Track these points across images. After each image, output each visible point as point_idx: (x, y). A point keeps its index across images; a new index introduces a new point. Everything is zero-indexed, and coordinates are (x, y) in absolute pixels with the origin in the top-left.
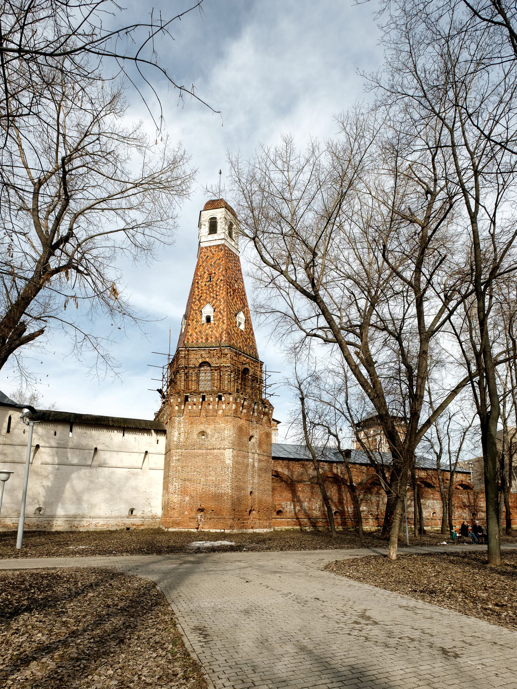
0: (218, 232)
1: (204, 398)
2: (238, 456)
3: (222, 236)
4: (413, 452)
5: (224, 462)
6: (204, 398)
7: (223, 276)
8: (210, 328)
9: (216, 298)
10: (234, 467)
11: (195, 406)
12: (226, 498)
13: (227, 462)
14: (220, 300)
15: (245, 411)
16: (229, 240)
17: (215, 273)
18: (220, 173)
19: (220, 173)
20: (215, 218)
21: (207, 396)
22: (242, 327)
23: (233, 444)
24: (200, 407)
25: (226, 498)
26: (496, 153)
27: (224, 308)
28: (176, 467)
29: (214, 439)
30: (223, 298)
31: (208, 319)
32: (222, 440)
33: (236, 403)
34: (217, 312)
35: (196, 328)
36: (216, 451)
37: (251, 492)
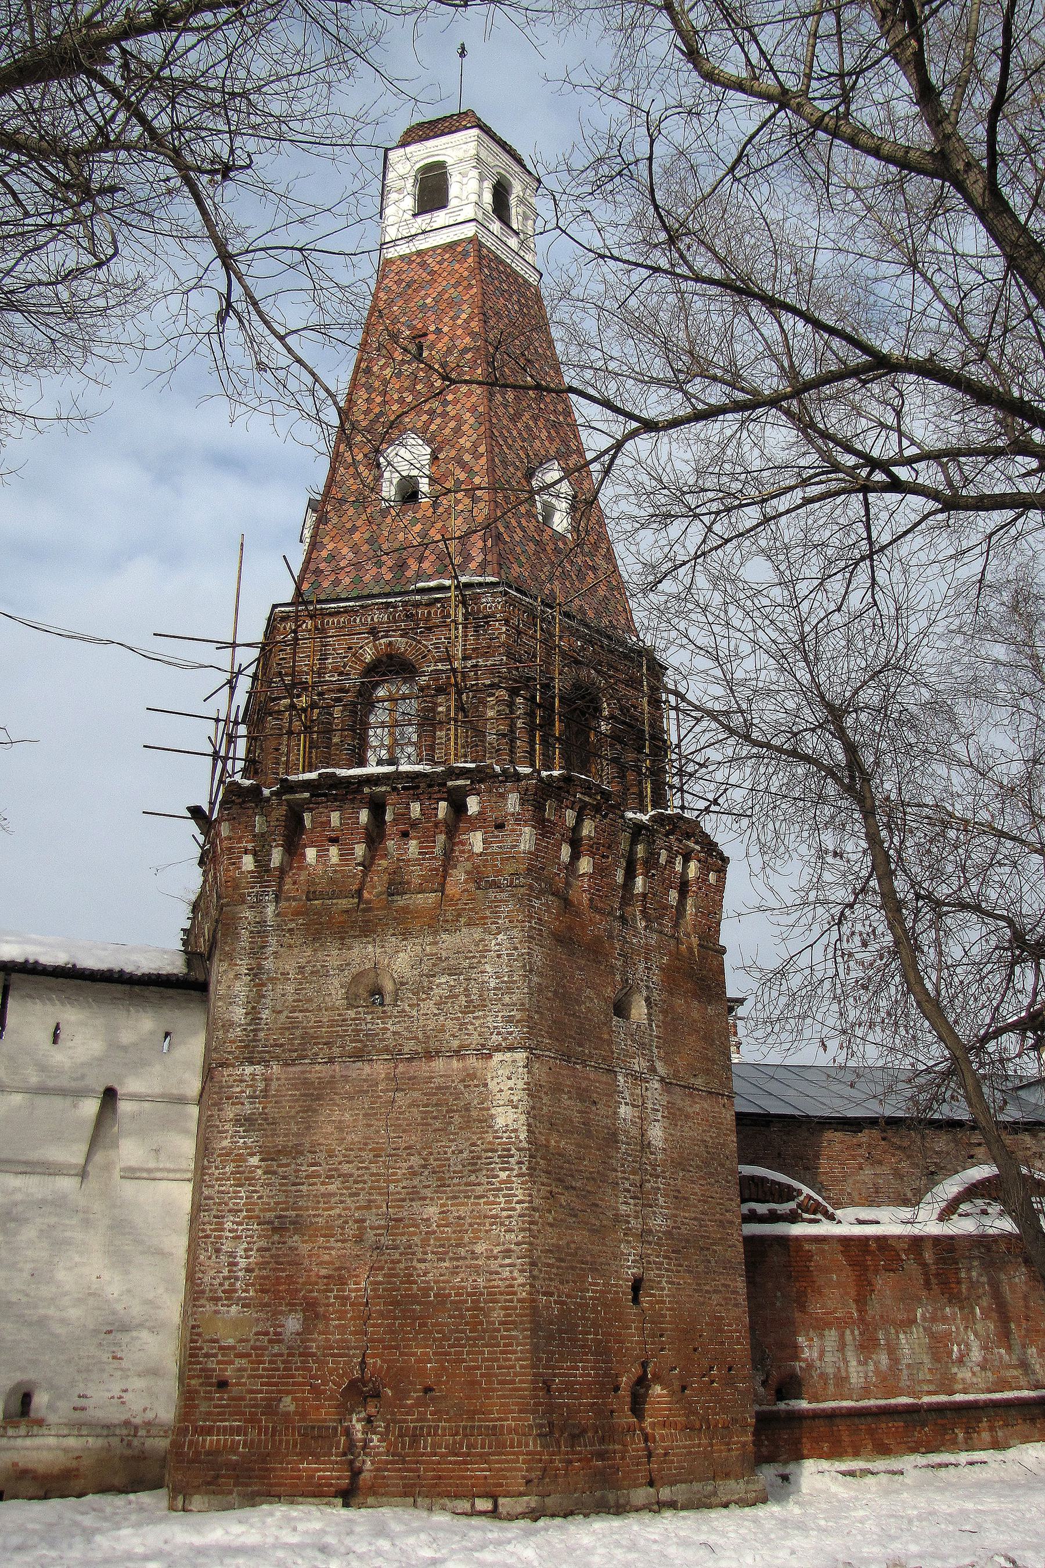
0: (453, 202)
1: (377, 808)
2: (556, 1089)
3: (469, 212)
4: (368, 846)
5: (486, 1121)
6: (377, 808)
7: (473, 335)
8: (415, 521)
9: (444, 415)
10: (536, 1149)
11: (334, 851)
12: (498, 1315)
13: (500, 1122)
14: (458, 418)
15: (585, 865)
16: (496, 226)
17: (439, 331)
18: (463, 53)
19: (463, 53)
20: (441, 165)
21: (392, 799)
22: (560, 522)
23: (532, 1029)
24: (360, 850)
25: (498, 1315)
26: (414, 1090)
27: (475, 446)
28: (240, 1159)
29: (429, 1006)
30: (473, 409)
31: (409, 494)
32: (469, 1008)
33: (543, 826)
34: (448, 460)
35: (354, 529)
36: (439, 1065)
37: (637, 1286)
